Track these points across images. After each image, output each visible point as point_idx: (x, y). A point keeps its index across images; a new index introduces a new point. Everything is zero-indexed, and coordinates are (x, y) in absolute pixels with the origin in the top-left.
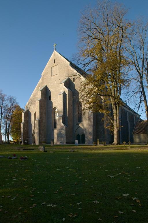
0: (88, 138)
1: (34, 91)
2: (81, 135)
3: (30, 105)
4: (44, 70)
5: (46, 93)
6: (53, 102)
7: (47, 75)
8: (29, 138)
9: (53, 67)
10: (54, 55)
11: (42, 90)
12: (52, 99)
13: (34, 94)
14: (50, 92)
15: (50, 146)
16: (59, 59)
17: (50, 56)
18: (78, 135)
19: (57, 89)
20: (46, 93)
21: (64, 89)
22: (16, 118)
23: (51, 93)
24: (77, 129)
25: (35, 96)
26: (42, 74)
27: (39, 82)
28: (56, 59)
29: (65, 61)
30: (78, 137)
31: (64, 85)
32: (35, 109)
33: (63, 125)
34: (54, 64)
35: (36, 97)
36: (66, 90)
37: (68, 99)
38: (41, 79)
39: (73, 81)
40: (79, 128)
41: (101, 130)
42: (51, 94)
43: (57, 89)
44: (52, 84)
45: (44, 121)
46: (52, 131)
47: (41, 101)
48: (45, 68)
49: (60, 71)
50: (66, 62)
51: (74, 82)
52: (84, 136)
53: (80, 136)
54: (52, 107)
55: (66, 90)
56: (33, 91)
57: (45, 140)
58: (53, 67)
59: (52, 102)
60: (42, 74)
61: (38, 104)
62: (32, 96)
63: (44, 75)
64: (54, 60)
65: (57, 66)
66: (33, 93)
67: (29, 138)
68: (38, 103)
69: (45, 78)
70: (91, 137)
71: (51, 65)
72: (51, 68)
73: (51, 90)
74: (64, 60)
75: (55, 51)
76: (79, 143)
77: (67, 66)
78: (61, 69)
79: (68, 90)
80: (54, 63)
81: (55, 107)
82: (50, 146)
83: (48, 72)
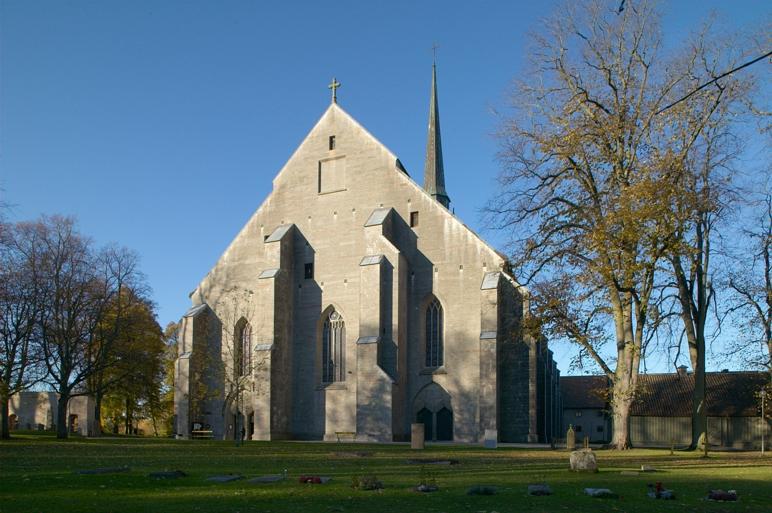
0: (46, 396)
1: (237, 239)
2: (437, 410)
3: (217, 289)
4: (285, 168)
5: (297, 255)
6: (322, 288)
7: (298, 189)
8: (208, 413)
9: (326, 160)
10: (332, 119)
11: (281, 240)
12: (319, 276)
13: (234, 249)
14: (313, 252)
15: (409, 450)
16: (353, 137)
17: (316, 122)
18: (425, 409)
19: (342, 244)
20: (297, 255)
21: (384, 246)
22: (112, 339)
23: (436, 275)
24: (422, 388)
25: (239, 259)
26: (277, 178)
27: (261, 210)
28: (340, 137)
29: (378, 149)
30: (424, 416)
31: (384, 234)
32: (256, 308)
33: (382, 373)
34: (332, 154)
35: (247, 262)
36: (393, 254)
37: (392, 280)
38: (269, 200)
39: (408, 223)
40: (430, 387)
41: (515, 398)
42: (316, 259)
43: (342, 244)
44: (319, 224)
45: (285, 355)
46: (316, 393)
47: (278, 278)
48: (290, 161)
49: (354, 180)
50: (380, 153)
51: (412, 226)
52: (446, 414)
53: (431, 414)
54: (321, 306)
55: (390, 251)
56: (235, 236)
57: (176, 416)
58: (326, 160)
59: (319, 288)
60: (277, 181)
61: (269, 290)
62: (226, 255)
63: (283, 187)
64: (332, 138)
65: (343, 161)
66: (231, 247)
67: (208, 413)
68: (268, 284)
69: (288, 195)
70: (495, 422)
71: (316, 153)
72: (318, 164)
73: (318, 242)
74: (372, 143)
75: (334, 106)
76: (428, 437)
77: (386, 168)
78: (360, 172)
79: (397, 252)
80: (331, 148)
81: (331, 306)
82: (409, 450)
83: (302, 175)
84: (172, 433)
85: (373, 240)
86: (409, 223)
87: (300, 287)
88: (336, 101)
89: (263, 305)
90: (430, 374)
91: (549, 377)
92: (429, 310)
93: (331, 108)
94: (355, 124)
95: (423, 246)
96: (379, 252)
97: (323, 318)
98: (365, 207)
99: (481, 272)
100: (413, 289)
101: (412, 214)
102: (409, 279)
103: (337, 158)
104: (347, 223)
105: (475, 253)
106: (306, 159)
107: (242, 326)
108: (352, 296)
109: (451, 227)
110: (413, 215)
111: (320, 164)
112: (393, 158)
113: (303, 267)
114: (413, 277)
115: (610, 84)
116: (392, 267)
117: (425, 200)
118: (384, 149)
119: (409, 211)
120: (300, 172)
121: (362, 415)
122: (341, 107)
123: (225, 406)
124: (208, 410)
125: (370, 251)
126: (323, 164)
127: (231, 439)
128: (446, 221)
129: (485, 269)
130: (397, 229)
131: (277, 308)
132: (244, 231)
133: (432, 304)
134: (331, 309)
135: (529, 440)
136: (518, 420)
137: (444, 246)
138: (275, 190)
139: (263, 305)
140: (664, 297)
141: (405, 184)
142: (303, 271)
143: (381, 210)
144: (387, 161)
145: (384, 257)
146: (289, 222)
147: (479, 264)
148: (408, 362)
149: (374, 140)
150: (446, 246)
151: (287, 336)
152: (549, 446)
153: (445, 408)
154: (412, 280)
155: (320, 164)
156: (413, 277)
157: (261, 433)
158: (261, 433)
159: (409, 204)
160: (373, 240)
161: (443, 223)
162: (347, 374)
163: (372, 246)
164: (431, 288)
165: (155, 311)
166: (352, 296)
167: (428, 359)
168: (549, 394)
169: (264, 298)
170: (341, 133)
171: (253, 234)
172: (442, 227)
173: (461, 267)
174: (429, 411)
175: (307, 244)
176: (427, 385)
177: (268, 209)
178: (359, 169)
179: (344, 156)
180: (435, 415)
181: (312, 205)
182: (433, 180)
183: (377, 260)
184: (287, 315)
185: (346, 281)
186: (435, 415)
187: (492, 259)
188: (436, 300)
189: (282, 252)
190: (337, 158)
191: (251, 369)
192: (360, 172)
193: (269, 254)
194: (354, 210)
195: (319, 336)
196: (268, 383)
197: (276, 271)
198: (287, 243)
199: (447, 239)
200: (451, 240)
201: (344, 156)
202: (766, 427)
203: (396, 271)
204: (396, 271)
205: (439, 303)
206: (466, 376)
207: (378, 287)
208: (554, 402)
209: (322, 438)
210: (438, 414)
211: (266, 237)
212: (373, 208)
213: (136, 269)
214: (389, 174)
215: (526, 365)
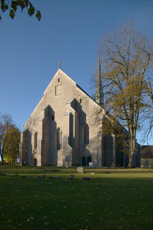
1: (35, 110)
5: (49, 113)
7: (50, 94)
10: (59, 74)
11: (44, 110)
12: (56, 119)
13: (34, 113)
18: (84, 157)
19: (61, 110)
20: (49, 113)
21: (71, 109)
23: (87, 117)
27: (41, 101)
29: (71, 81)
32: (38, 129)
34: (59, 83)
36: (73, 111)
38: (43, 98)
40: (85, 150)
43: (61, 110)
45: (46, 142)
48: (48, 87)
50: (71, 82)
55: (73, 111)
58: (57, 86)
60: (45, 93)
61: (41, 124)
63: (46, 94)
64: (59, 79)
65: (62, 85)
66: (33, 112)
68: (40, 123)
69: (47, 96)
73: (55, 109)
75: (59, 70)
77: (73, 86)
78: (66, 88)
79: (74, 111)
80: (59, 82)
85: (68, 108)
86: (79, 102)
88: (60, 68)
89: (39, 128)
90: (85, 147)
92: (85, 128)
93: (59, 70)
94: (65, 74)
95: (84, 109)
96: (70, 112)
97: (56, 132)
98: (67, 98)
100: (80, 122)
101: (80, 99)
102: (79, 119)
103: (60, 85)
104: (63, 103)
106: (52, 86)
107: (36, 134)
108: (63, 124)
110: (80, 100)
111: (56, 87)
112: (76, 83)
113: (52, 117)
114: (80, 118)
115: (121, 56)
116: (73, 116)
118: (72, 81)
119: (79, 99)
120: (51, 90)
121: (67, 160)
122: (62, 70)
123: (32, 157)
124: (28, 158)
125: (67, 111)
126: (57, 87)
127: (34, 166)
130: (75, 104)
131: (43, 129)
132: (37, 108)
133: (86, 126)
134: (59, 129)
137: (89, 108)
138: (44, 96)
139: (39, 128)
141: (78, 91)
142: (51, 118)
144: (73, 84)
145: (71, 113)
146: (48, 104)
148: (79, 143)
149: (70, 79)
150: (90, 108)
151: (47, 137)
152: (108, 167)
153: (89, 157)
154: (79, 118)
155: (56, 87)
157: (39, 164)
158: (39, 164)
159: (79, 97)
160: (68, 108)
163: (68, 110)
164: (86, 121)
166: (63, 124)
167: (85, 142)
169: (40, 126)
170: (61, 77)
171: (39, 108)
174: (85, 158)
175: (53, 110)
176: (84, 150)
177: (43, 101)
178: (66, 87)
179: (62, 84)
180: (87, 159)
183: (69, 114)
184: (47, 131)
185: (62, 120)
186: (87, 159)
188: (87, 125)
189: (45, 113)
190: (60, 85)
191: (130, 138)
192: (66, 88)
193: (42, 114)
194: (64, 99)
195: (56, 136)
196: (147, 145)
197: (43, 119)
198: (47, 110)
199: (90, 106)
200: (91, 107)
201: (62, 84)
203: (74, 117)
204: (74, 117)
205: (88, 125)
206: (94, 147)
207: (69, 122)
208: (141, 153)
209: (57, 165)
210: (88, 158)
212: (70, 98)
213: (12, 119)
214: (74, 88)
215: (112, 143)
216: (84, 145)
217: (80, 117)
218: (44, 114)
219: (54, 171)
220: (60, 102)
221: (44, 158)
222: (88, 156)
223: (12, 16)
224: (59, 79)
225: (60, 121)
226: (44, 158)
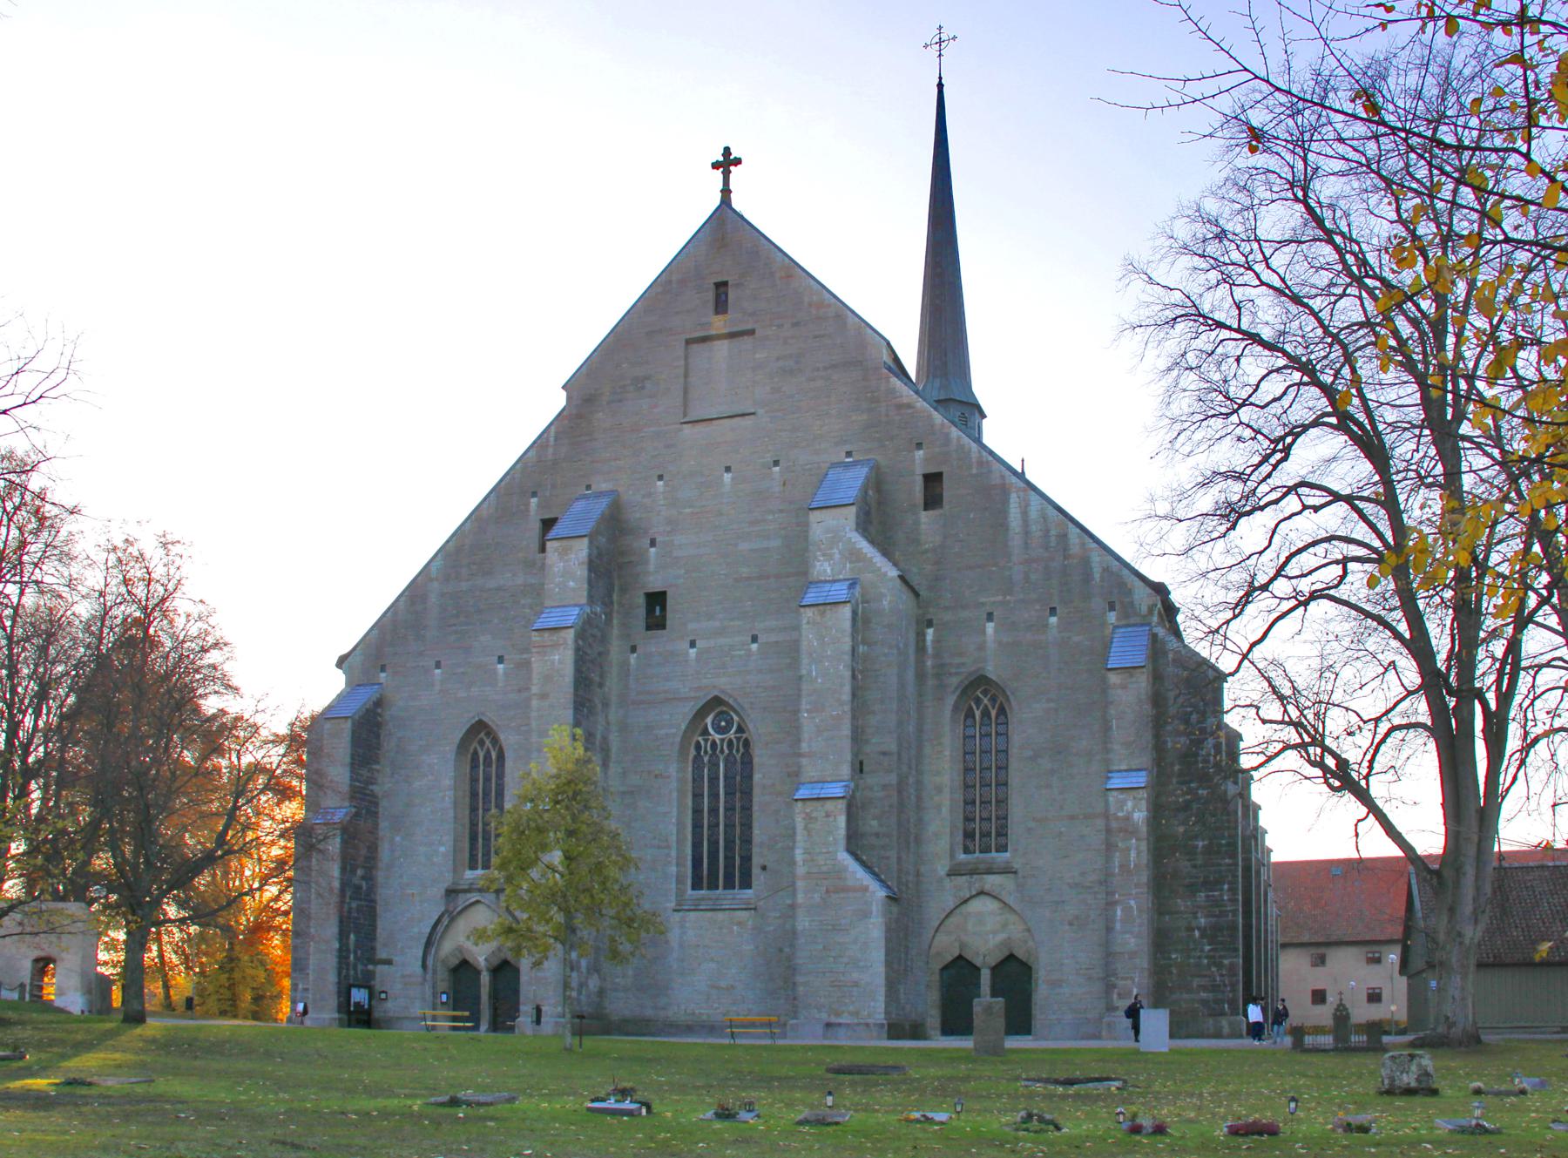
11: (592, 537)
18: (960, 957)
19: (744, 546)
34: (719, 324)
43: (744, 546)
46: (677, 916)
53: (978, 969)
68: (555, 646)
84: (22, 997)
87: (633, 649)
91: (1258, 873)
99: (1104, 624)
103: (732, 335)
105: (1087, 577)
109: (1025, 514)
113: (641, 601)
117: (961, 447)
128: (1013, 497)
129: (1112, 617)
135: (1226, 1030)
136: (1196, 982)
140: (1538, 692)
141: (909, 406)
143: (847, 466)
147: (1098, 603)
156: (930, 631)
161: (1006, 502)
162: (756, 871)
163: (829, 557)
165: (307, 714)
168: (1258, 918)
169: (547, 678)
172: (1003, 513)
173: (1053, 611)
176: (965, 902)
179: (751, 332)
181: (668, 446)
182: (708, 344)
185: (754, 639)
186: (985, 976)
187: (1130, 592)
190: (732, 335)
194: (776, 463)
198: (602, 540)
199: (1016, 541)
200: (1026, 545)
201: (751, 332)
202: (561, 882)
210: (994, 969)
211: (548, 524)
216: (962, 857)
217: (930, 624)
218: (582, 572)
219: (1459, 870)
220: (727, 477)
221: (584, 963)
222: (1000, 956)
223: (1132, 268)
224: (721, 286)
225: (722, 641)
226: (584, 963)
